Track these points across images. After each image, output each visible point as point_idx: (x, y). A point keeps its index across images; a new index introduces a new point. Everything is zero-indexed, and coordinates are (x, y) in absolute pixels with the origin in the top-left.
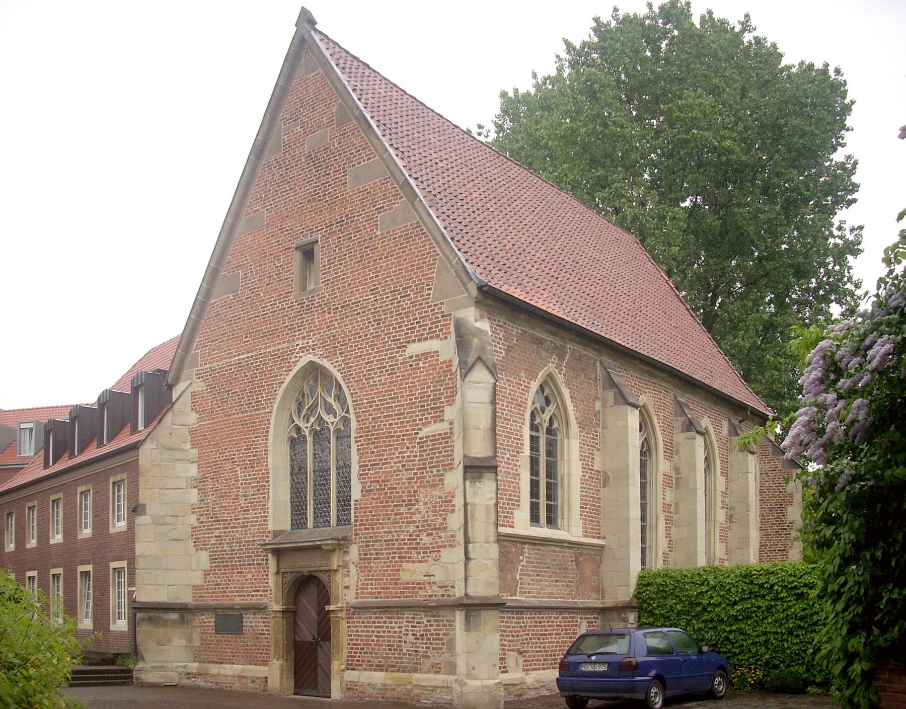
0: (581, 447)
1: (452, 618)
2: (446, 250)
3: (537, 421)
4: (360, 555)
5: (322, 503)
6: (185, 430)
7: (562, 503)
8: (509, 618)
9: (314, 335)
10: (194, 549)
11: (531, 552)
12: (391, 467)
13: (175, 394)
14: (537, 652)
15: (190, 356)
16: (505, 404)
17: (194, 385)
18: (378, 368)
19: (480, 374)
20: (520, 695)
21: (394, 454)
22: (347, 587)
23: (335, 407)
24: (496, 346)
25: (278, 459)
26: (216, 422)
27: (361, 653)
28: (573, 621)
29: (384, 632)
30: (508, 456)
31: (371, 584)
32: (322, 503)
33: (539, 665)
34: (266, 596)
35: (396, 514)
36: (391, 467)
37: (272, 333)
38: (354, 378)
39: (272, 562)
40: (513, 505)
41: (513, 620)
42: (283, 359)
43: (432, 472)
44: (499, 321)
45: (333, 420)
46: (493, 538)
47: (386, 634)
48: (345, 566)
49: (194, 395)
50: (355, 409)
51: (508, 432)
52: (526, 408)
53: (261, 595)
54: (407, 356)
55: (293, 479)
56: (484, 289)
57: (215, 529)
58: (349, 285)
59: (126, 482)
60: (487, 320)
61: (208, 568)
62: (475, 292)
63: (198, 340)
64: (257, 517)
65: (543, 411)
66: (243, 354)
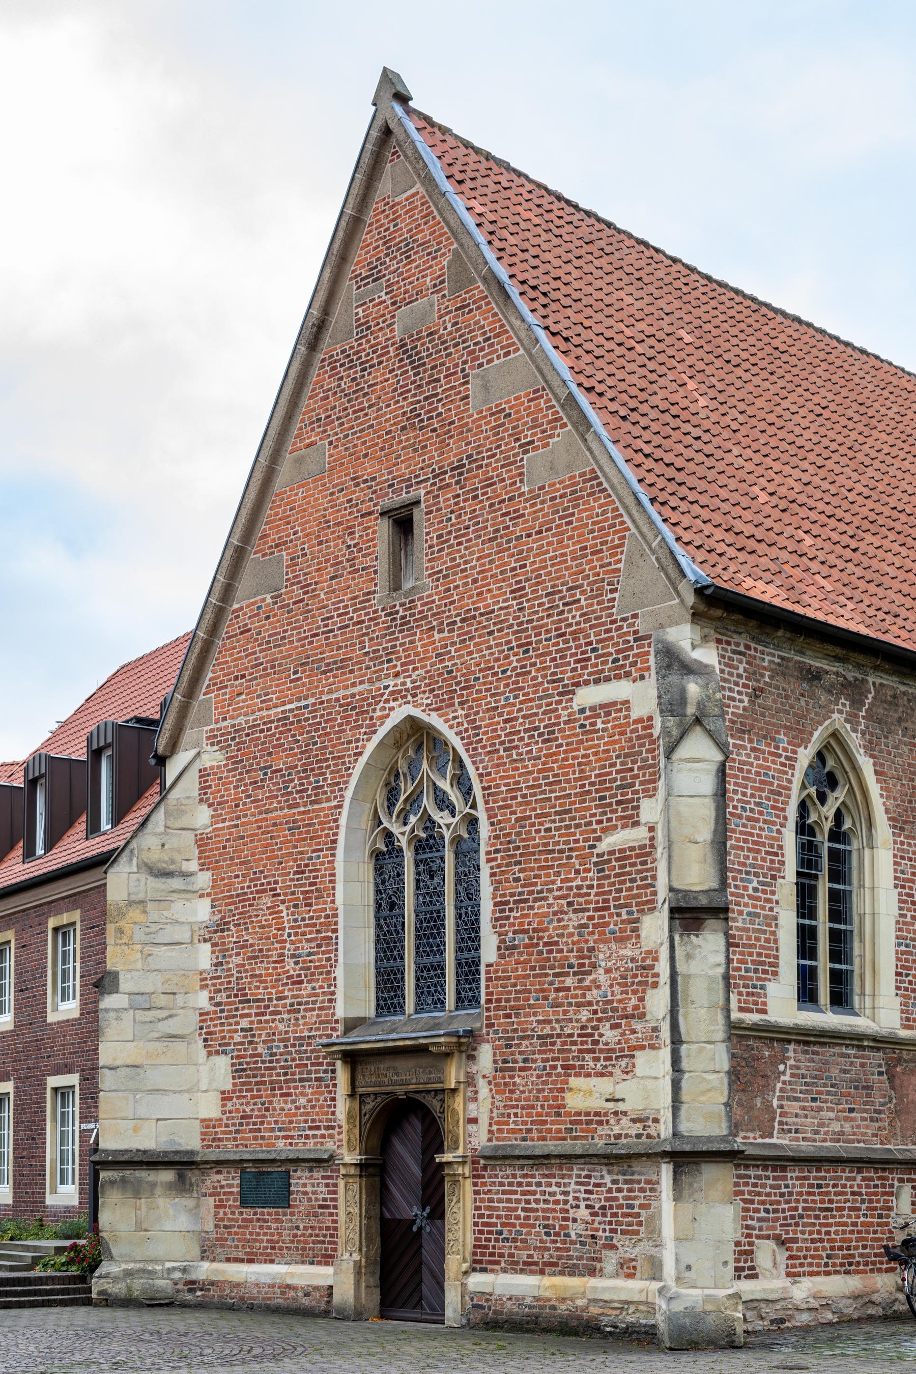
0: (895, 863)
1: (655, 1178)
2: (642, 522)
3: (813, 818)
4: (495, 1062)
5: (429, 975)
6: (190, 837)
7: (862, 966)
8: (758, 1177)
9: (415, 669)
10: (204, 1053)
11: (801, 1057)
12: (549, 906)
13: (172, 770)
14: (813, 1241)
15: (195, 704)
16: (749, 791)
17: (204, 757)
18: (526, 731)
19: (699, 749)
20: (782, 1321)
21: (553, 882)
22: (474, 1121)
23: (453, 798)
24: (730, 690)
25: (351, 890)
26: (243, 824)
27: (497, 1240)
28: (884, 1186)
29: (537, 1201)
30: (755, 884)
31: (516, 1115)
32: (429, 975)
33: (818, 1265)
34: (331, 1136)
35: (557, 990)
36: (549, 906)
37: (342, 665)
38: (484, 747)
39: (342, 1075)
40: (765, 972)
41: (768, 1181)
42: (360, 712)
43: (619, 915)
44: (737, 645)
45: (450, 820)
46: (720, 1035)
47: (542, 1205)
48: (470, 1081)
49: (203, 774)
50: (487, 803)
51: (755, 843)
52: (789, 796)
53: (323, 1136)
54: (576, 708)
55: (379, 926)
56: (709, 592)
57: (242, 1016)
58: (475, 581)
59: (78, 927)
60: (713, 645)
61: (229, 1087)
62: (690, 599)
63: (210, 675)
64: (317, 995)
65: (822, 798)
66: (291, 702)
